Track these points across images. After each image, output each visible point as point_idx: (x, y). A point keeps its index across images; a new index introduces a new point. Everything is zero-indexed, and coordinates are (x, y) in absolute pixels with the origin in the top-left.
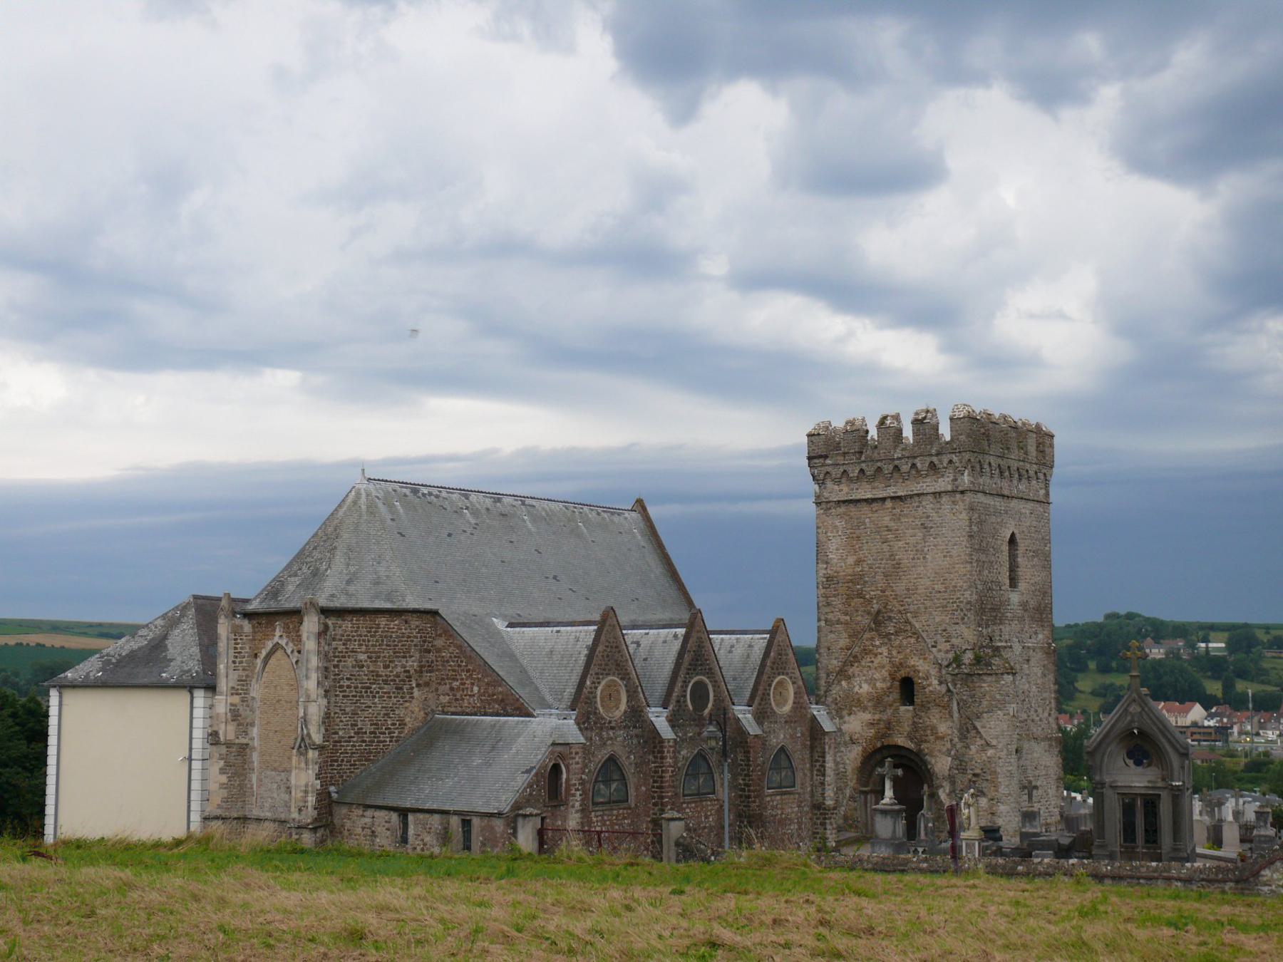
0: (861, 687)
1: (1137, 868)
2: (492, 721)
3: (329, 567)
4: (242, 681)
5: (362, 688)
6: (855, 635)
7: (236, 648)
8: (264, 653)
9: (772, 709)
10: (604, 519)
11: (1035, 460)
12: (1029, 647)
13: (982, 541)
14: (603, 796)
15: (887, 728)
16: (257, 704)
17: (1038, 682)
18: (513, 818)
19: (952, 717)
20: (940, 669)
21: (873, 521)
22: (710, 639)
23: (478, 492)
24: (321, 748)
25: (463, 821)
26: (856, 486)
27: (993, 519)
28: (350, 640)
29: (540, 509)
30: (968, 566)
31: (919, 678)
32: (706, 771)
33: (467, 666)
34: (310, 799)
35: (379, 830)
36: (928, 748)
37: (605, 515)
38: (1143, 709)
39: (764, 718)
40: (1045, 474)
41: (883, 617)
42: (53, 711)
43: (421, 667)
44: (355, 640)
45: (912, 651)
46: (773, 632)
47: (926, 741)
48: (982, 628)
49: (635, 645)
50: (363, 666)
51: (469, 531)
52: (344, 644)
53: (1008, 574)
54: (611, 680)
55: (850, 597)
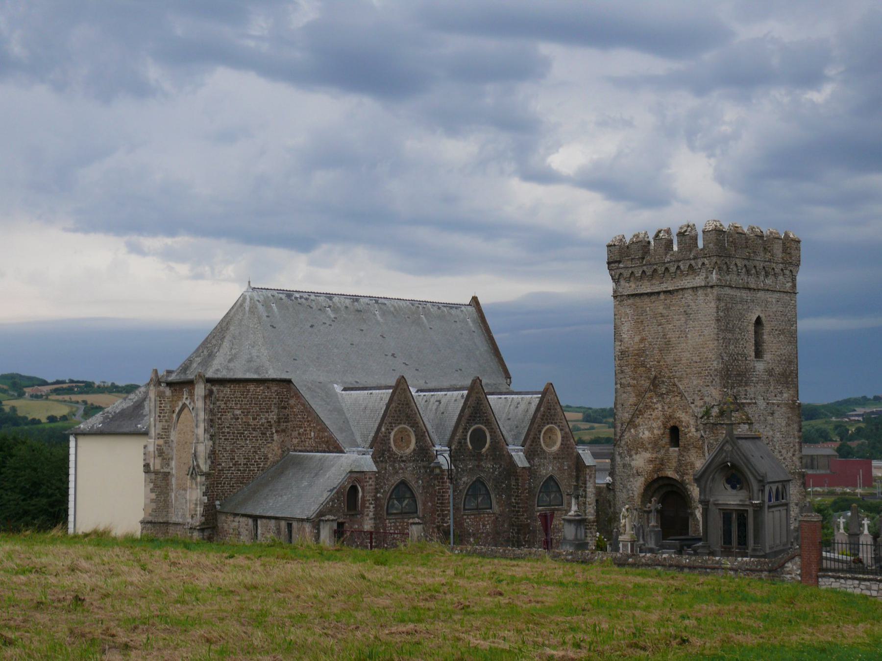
0: (644, 434)
1: (706, 561)
2: (321, 456)
3: (219, 350)
4: (165, 429)
5: (238, 433)
6: (640, 395)
7: (160, 407)
8: (177, 410)
9: (542, 448)
10: (443, 311)
11: (781, 260)
12: (773, 404)
13: (728, 323)
14: (397, 509)
15: (661, 464)
16: (174, 445)
17: (783, 430)
18: (316, 522)
19: (704, 455)
20: (697, 420)
21: (652, 310)
22: (487, 398)
23: (341, 295)
24: (207, 475)
25: (288, 523)
26: (640, 283)
27: (740, 306)
28: (229, 401)
29: (390, 306)
30: (716, 342)
31: (683, 427)
32: (484, 492)
33: (307, 418)
34: (198, 509)
35: (242, 530)
36: (688, 479)
37: (445, 309)
38: (733, 448)
39: (534, 455)
40: (791, 271)
41: (659, 381)
42: (72, 451)
43: (279, 419)
44: (233, 401)
45: (678, 406)
46: (544, 393)
47: (687, 474)
48: (728, 389)
49: (438, 403)
50: (238, 418)
51: (328, 323)
52: (225, 404)
53: (753, 348)
54: (402, 428)
55: (636, 367)
